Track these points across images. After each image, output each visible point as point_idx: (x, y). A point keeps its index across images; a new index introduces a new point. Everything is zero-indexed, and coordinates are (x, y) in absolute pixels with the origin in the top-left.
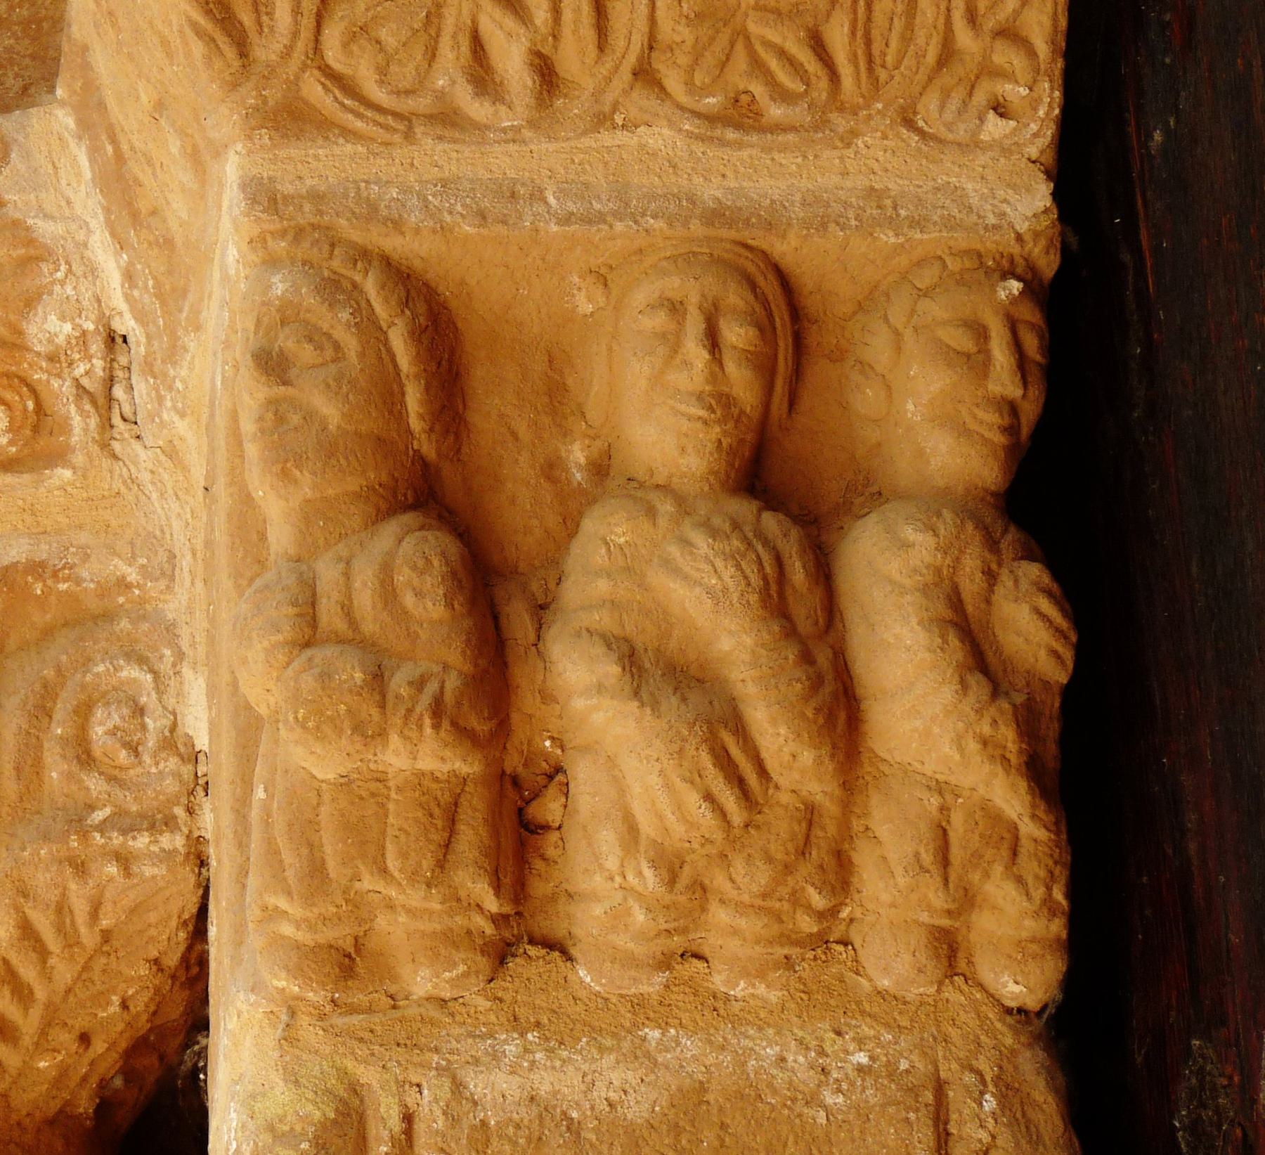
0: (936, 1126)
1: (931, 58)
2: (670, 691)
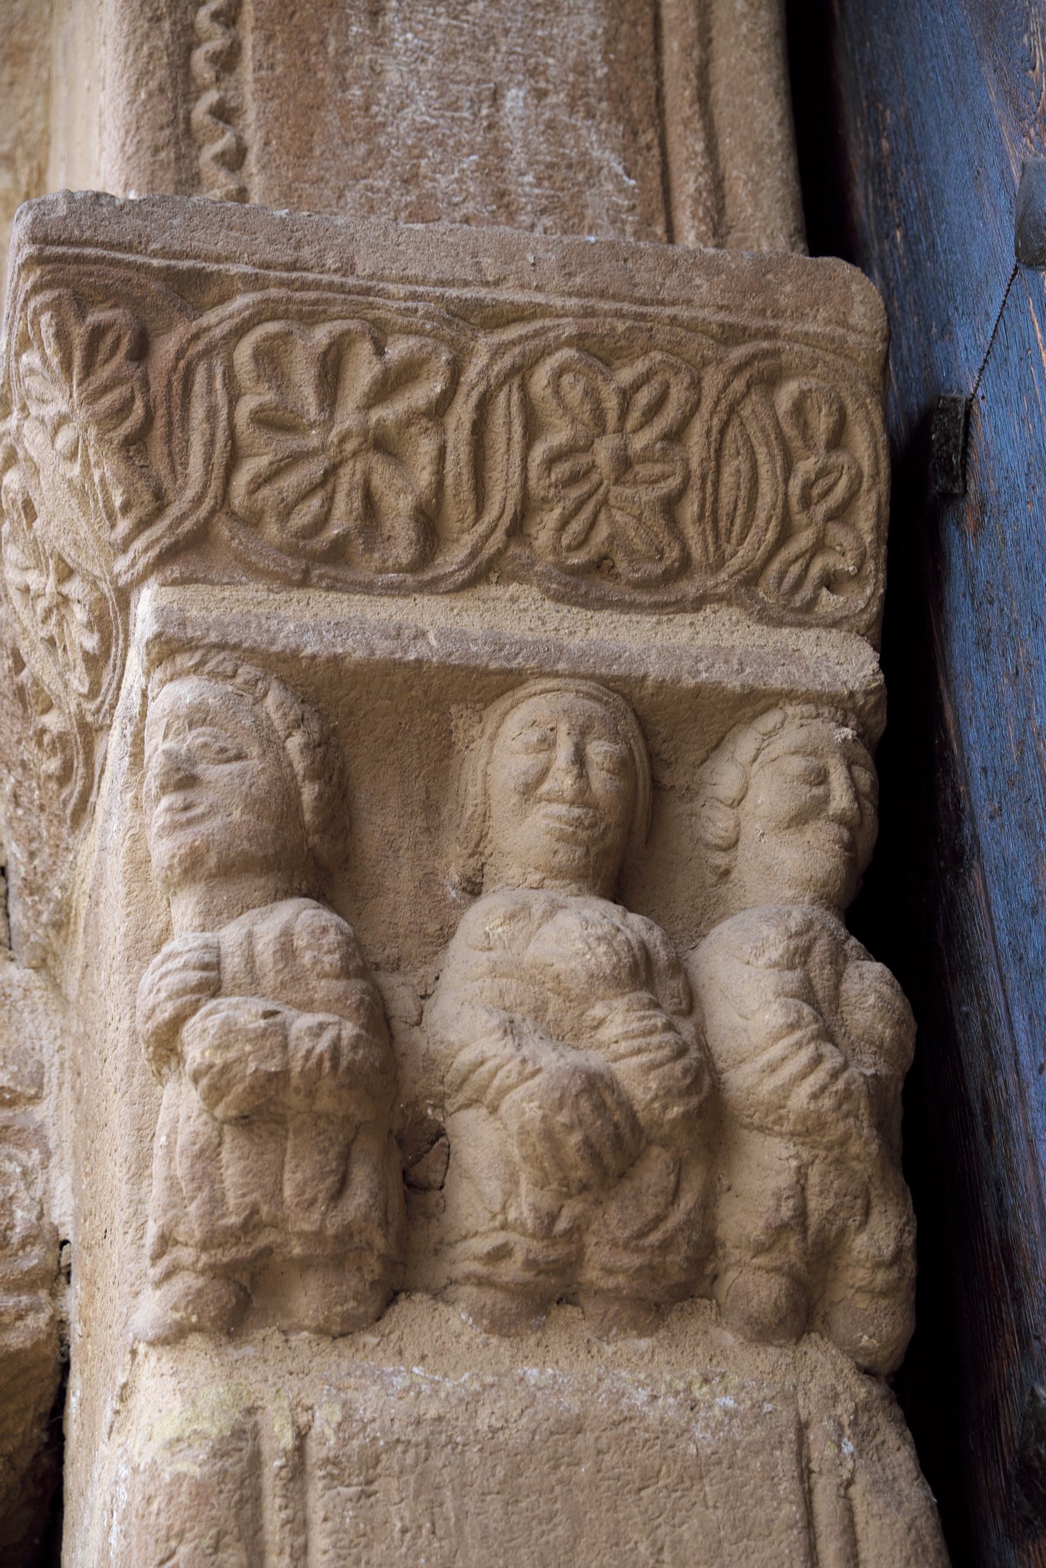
0: (799, 1461)
1: (770, 536)
2: (549, 1049)
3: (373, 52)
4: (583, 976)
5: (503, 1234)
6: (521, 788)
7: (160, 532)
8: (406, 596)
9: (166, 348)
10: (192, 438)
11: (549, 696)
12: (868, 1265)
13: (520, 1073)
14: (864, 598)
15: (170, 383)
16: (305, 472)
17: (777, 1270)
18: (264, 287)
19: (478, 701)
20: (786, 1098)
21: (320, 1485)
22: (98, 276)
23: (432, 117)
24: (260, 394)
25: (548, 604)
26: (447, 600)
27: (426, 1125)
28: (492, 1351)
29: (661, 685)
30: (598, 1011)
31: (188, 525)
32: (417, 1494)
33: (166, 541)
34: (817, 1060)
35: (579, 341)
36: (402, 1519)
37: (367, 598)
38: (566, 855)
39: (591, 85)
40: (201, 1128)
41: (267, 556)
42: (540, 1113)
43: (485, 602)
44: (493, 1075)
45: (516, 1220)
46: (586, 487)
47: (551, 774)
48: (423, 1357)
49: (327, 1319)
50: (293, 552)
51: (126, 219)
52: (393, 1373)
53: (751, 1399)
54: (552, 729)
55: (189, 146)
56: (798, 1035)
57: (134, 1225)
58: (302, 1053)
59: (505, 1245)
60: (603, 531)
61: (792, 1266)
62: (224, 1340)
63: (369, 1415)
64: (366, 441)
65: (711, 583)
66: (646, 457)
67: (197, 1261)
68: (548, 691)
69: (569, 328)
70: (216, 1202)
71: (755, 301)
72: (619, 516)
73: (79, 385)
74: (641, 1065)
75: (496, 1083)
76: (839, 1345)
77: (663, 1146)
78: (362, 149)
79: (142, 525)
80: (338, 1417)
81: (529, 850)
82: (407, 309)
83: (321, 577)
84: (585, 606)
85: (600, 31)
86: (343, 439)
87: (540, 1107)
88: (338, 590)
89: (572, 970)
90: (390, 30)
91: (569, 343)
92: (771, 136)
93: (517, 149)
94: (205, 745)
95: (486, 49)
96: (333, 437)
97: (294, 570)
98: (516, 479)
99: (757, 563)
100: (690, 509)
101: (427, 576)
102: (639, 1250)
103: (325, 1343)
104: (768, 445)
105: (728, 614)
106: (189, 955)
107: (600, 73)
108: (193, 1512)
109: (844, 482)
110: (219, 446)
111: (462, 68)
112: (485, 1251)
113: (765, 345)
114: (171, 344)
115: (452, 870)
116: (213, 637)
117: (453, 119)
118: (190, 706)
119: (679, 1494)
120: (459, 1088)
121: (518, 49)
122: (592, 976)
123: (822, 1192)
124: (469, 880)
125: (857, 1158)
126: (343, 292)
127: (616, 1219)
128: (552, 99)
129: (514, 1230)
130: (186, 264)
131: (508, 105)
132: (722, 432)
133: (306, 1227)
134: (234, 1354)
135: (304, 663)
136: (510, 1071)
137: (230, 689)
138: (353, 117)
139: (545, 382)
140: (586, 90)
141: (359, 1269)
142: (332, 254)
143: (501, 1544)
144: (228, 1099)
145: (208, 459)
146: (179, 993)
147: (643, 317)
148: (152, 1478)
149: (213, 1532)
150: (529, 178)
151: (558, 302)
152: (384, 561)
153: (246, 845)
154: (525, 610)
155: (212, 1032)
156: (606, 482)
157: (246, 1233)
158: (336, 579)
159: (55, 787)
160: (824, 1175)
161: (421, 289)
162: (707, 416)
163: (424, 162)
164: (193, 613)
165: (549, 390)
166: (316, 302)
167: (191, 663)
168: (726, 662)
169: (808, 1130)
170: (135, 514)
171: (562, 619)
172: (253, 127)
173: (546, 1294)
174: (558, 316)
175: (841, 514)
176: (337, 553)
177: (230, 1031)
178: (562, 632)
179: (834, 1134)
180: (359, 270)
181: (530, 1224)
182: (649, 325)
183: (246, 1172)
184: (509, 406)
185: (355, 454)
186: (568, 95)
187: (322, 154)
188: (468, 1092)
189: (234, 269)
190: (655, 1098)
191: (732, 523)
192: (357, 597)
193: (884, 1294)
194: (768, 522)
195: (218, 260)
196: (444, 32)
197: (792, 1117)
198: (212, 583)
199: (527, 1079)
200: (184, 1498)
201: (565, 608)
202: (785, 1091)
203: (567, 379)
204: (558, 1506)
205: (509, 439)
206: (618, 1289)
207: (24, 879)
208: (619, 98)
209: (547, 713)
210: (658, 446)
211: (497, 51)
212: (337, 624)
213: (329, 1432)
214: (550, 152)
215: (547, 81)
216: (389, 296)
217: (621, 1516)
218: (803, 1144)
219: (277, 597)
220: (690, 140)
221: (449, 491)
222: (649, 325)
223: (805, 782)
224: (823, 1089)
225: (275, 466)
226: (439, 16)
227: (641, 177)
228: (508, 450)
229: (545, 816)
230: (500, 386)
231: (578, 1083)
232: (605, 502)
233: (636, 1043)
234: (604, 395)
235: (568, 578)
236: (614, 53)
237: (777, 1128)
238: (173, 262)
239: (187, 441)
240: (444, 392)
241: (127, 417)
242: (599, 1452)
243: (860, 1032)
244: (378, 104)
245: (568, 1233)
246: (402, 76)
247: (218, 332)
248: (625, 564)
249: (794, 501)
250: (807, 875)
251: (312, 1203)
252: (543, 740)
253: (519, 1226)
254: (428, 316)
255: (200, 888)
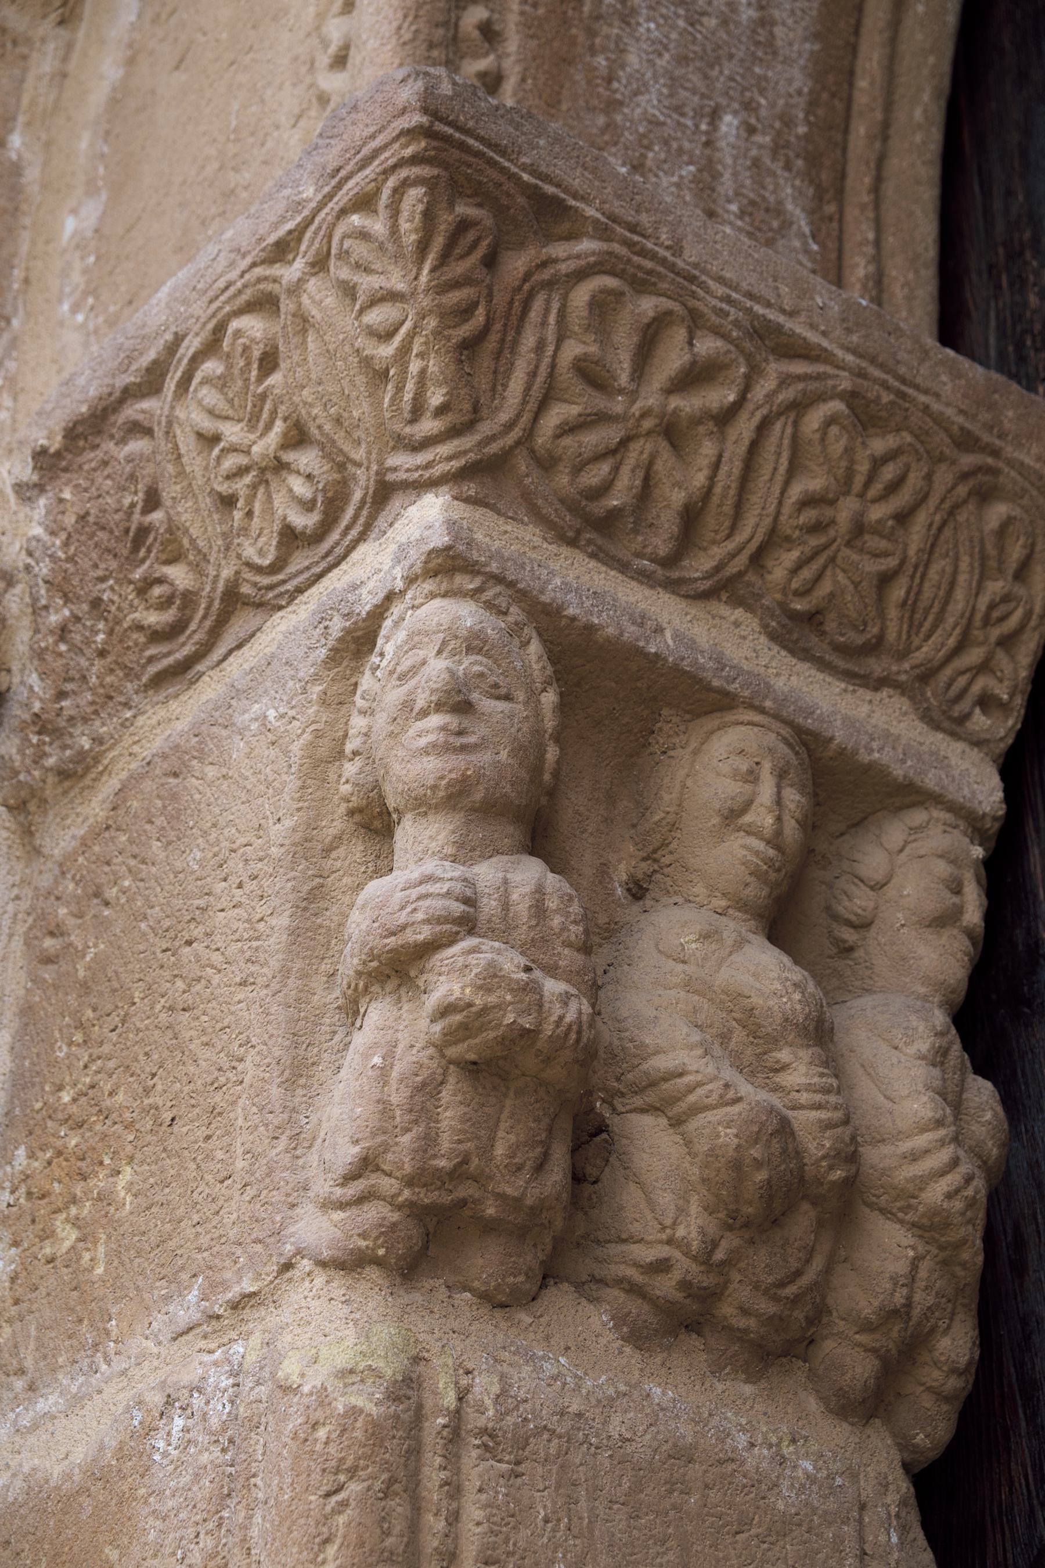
1: (952, 642)
3: (621, 28)
4: (778, 1018)
5: (667, 1248)
6: (726, 812)
7: (468, 446)
8: (652, 587)
9: (516, 264)
10: (517, 363)
11: (756, 729)
12: (945, 1368)
13: (721, 1097)
14: (1003, 728)
15: (511, 303)
16: (604, 434)
17: (874, 1351)
18: (609, 240)
19: (688, 712)
20: (921, 1189)
21: (475, 1453)
22: (476, 171)
23: (662, 113)
24: (584, 343)
25: (763, 639)
26: (683, 604)
27: (592, 1116)
28: (626, 1360)
29: (842, 752)
30: (784, 1055)
31: (494, 448)
32: (559, 1486)
33: (472, 456)
34: (955, 1162)
35: (851, 397)
36: (545, 1507)
37: (621, 577)
38: (756, 892)
39: (793, 139)
40: (426, 1061)
41: (551, 504)
42: (736, 1141)
43: (713, 618)
44: (691, 1089)
45: (684, 1238)
46: (823, 540)
47: (753, 807)
48: (567, 1348)
49: (497, 1287)
50: (574, 508)
51: (500, 121)
52: (543, 1358)
53: (828, 1469)
54: (757, 763)
55: (455, 53)
56: (942, 1132)
57: (288, 1133)
58: (554, 1018)
59: (667, 1260)
60: (825, 588)
61: (888, 1351)
62: (398, 1280)
63: (522, 1394)
64: (660, 425)
65: (894, 668)
66: (877, 530)
67: (399, 1194)
68: (750, 723)
69: (845, 383)
70: (429, 1140)
71: (985, 416)
72: (841, 577)
73: (433, 270)
74: (820, 1121)
75: (692, 1098)
76: (894, 1436)
77: (813, 1203)
78: (601, 120)
79: (453, 432)
80: (496, 1389)
81: (721, 874)
82: (721, 310)
83: (589, 542)
84: (792, 652)
85: (806, 90)
86: (645, 414)
87: (737, 1136)
88: (599, 560)
89: (769, 1009)
90: (638, 13)
91: (843, 396)
92: (926, 249)
93: (727, 176)
94: (481, 675)
95: (712, 67)
96: (636, 409)
97: (570, 527)
98: (772, 509)
99: (936, 663)
100: (898, 592)
101: (675, 575)
102: (776, 1299)
103: (484, 1310)
104: (971, 556)
105: (901, 703)
106: (452, 884)
107: (802, 130)
108: (367, 1450)
109: (1019, 614)
110: (540, 379)
111: (690, 76)
112: (648, 1260)
113: (990, 461)
114: (520, 263)
115: (622, 866)
116: (494, 567)
117: (679, 123)
118: (470, 630)
119: (766, 1546)
120: (639, 1090)
121: (738, 78)
122: (786, 1020)
123: (926, 1288)
124: (637, 883)
125: (963, 1265)
126: (673, 272)
127: (761, 1261)
128: (758, 138)
129: (678, 1247)
130: (550, 189)
131: (724, 128)
132: (940, 530)
133: (509, 1191)
134: (406, 1299)
135: (564, 622)
136: (711, 1091)
137: (503, 625)
138: (597, 85)
139: (816, 426)
140: (788, 142)
141: (535, 1245)
142: (665, 229)
143: (624, 1556)
144: (473, 1042)
145: (527, 390)
146: (439, 920)
147: (902, 395)
148: (321, 1404)
149: (385, 1476)
150: (734, 208)
151: (840, 353)
152: (645, 547)
153: (508, 789)
154: (744, 638)
155: (475, 971)
156: (839, 540)
157: (451, 1180)
158: (600, 549)
159: (142, 640)
160: (932, 1271)
161: (734, 295)
162: (932, 510)
163: (651, 155)
164: (479, 536)
165: (818, 436)
166: (650, 272)
167: (471, 586)
168: (894, 748)
169: (930, 1227)
170: (449, 419)
171: (773, 657)
172: (513, 58)
173: (680, 1319)
174: (838, 367)
175: (1007, 642)
176: (607, 524)
177: (495, 976)
178: (770, 671)
179: (953, 1236)
180: (686, 254)
181: (695, 1245)
182: (907, 405)
183: (464, 1119)
184: (781, 438)
185: (649, 433)
186: (773, 141)
187: (569, 110)
188: (651, 1097)
189: (590, 212)
190: (824, 1157)
191: (925, 619)
192: (613, 573)
193: (947, 1399)
194: (954, 628)
195: (575, 196)
196: (680, 34)
197: (921, 1208)
198: (499, 513)
199: (727, 1104)
200: (358, 1434)
201: (776, 648)
202: (923, 1182)
203: (834, 430)
204: (670, 1531)
205: (775, 469)
206: (746, 1331)
207: (36, 715)
208: (813, 160)
209: (755, 746)
210: (890, 523)
211: (721, 72)
212: (595, 593)
213: (488, 1402)
214: (753, 190)
215: (758, 119)
216: (708, 291)
217: (721, 1555)
218: (921, 1237)
219: (550, 547)
220: (864, 227)
221: (715, 500)
222: (907, 405)
223: (947, 887)
224: (957, 1191)
225: (582, 419)
226: (678, 16)
227: (822, 245)
228: (771, 480)
229: (744, 846)
230: (779, 414)
231: (773, 1125)
232: (832, 559)
233: (818, 1097)
234: (858, 457)
235: (787, 621)
236: (815, 116)
237: (900, 1215)
238: (540, 183)
239: (512, 364)
240: (735, 403)
241: (466, 321)
242: (707, 1486)
243: (974, 1143)
244: (619, 82)
245: (723, 1263)
246: (641, 62)
247: (563, 268)
248: (834, 625)
249: (978, 617)
250: (941, 977)
251: (520, 1168)
252: (750, 772)
253: (682, 1245)
254: (736, 323)
255: (458, 818)
